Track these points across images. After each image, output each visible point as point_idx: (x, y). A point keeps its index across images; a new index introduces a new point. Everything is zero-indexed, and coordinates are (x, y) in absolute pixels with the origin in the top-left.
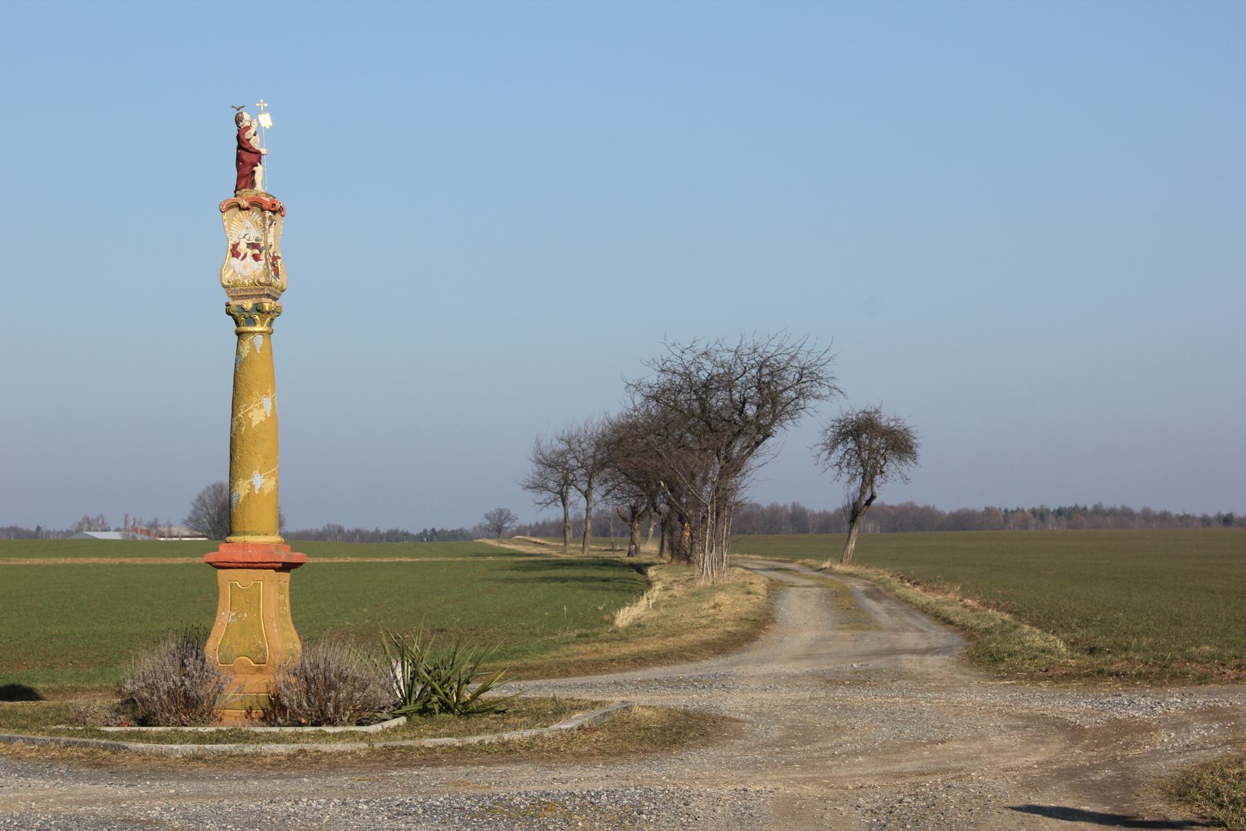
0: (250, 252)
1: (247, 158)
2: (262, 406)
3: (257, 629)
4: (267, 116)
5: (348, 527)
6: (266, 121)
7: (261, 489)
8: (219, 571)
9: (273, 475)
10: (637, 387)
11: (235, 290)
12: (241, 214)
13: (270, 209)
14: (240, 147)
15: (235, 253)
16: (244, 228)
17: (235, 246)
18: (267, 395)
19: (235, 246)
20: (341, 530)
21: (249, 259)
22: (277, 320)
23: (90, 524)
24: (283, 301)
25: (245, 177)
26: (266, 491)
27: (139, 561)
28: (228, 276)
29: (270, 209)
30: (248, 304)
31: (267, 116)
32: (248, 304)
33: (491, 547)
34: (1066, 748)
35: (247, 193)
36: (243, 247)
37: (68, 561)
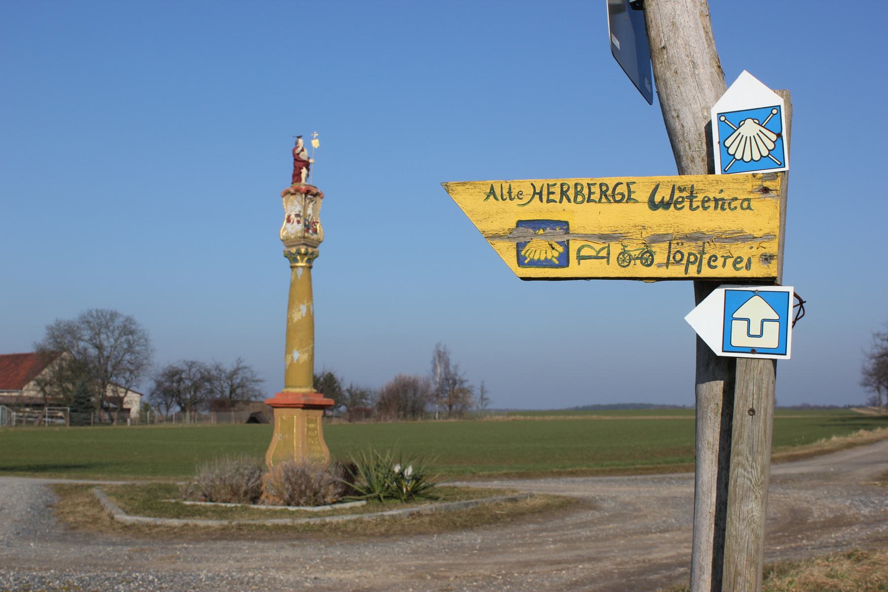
0: (296, 219)
1: (300, 164)
2: (299, 310)
3: (298, 442)
4: (317, 141)
5: (812, 404)
6: (315, 143)
7: (298, 360)
8: (276, 410)
9: (306, 351)
10: (878, 335)
11: (287, 242)
12: (292, 197)
13: (310, 194)
14: (295, 160)
15: (289, 221)
16: (293, 206)
17: (289, 217)
18: (304, 303)
19: (289, 217)
20: (808, 406)
21: (295, 223)
22: (315, 263)
23: (850, 407)
24: (320, 248)
25: (297, 176)
26: (301, 362)
27: (681, 417)
28: (283, 234)
29: (310, 194)
30: (294, 250)
31: (317, 141)
32: (294, 250)
33: (862, 414)
34: (273, 485)
35: (296, 185)
36: (293, 216)
37: (664, 417)
